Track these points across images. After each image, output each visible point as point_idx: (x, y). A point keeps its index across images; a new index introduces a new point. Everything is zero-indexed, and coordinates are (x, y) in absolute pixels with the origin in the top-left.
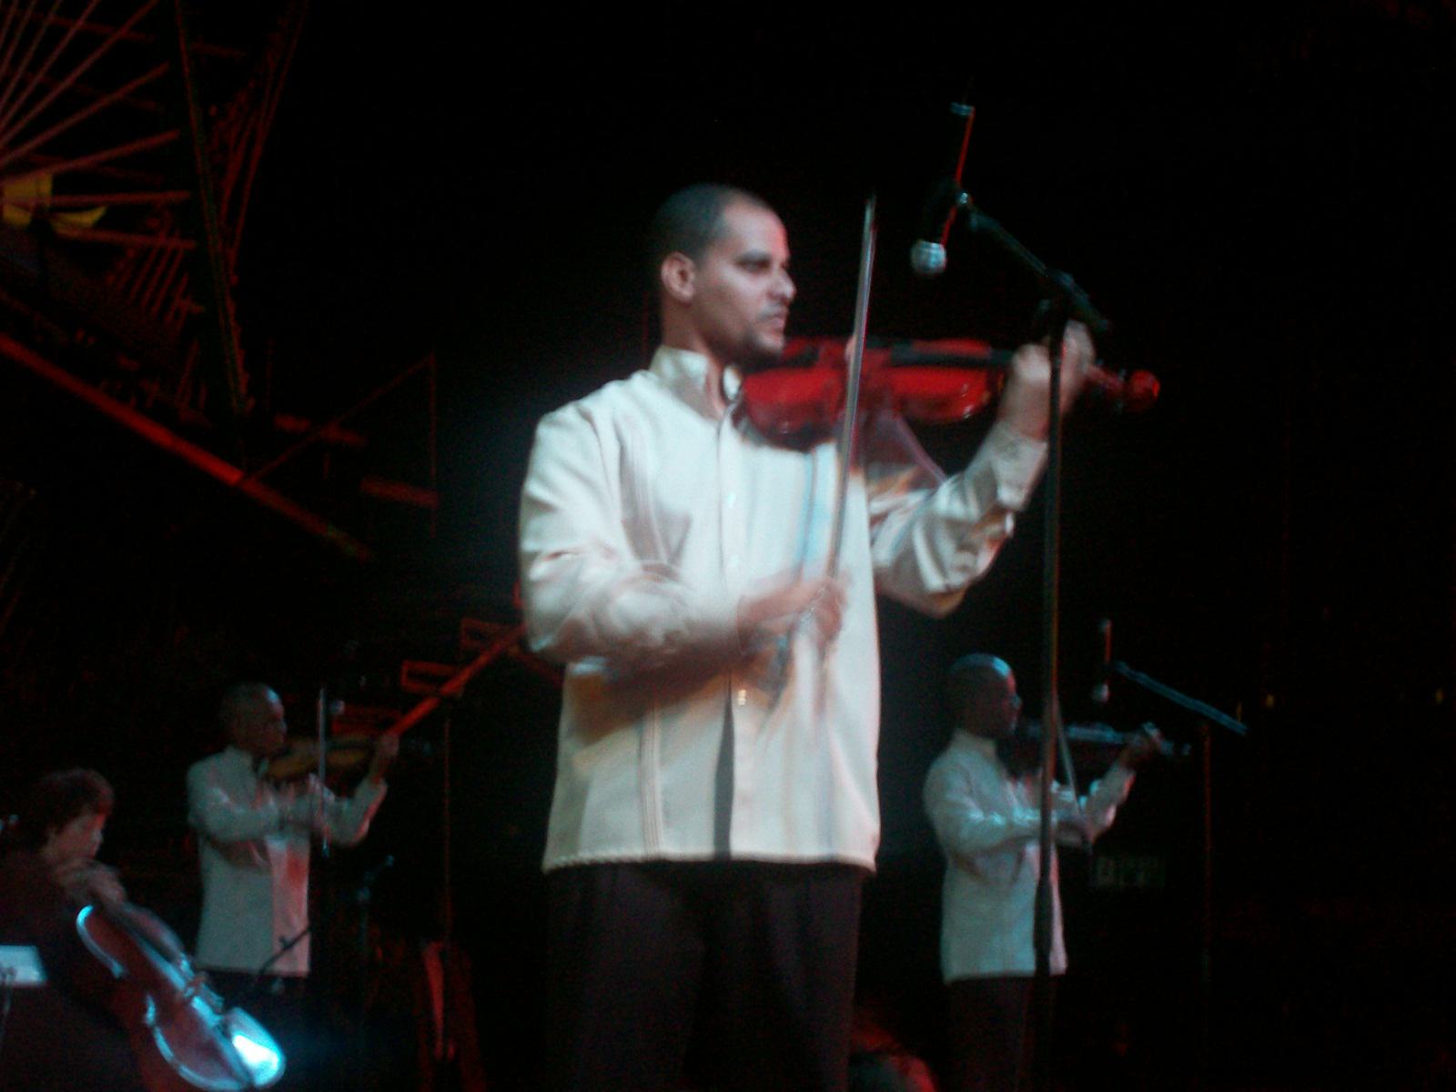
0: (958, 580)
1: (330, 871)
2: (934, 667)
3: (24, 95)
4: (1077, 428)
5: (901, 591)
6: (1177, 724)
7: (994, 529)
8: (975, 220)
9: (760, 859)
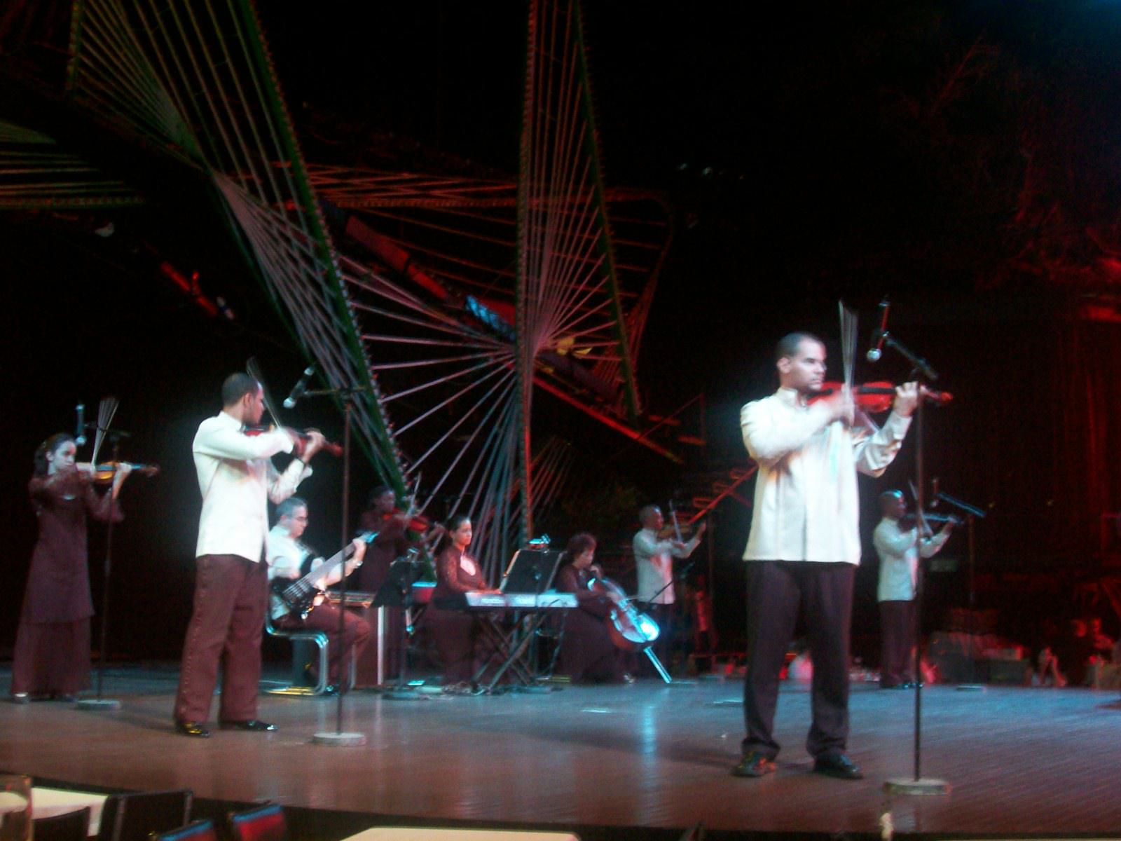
0: (882, 465)
1: (678, 565)
2: (875, 496)
3: (564, 312)
4: (923, 412)
5: (864, 471)
6: (960, 513)
7: (893, 448)
8: (890, 342)
9: (497, 606)
